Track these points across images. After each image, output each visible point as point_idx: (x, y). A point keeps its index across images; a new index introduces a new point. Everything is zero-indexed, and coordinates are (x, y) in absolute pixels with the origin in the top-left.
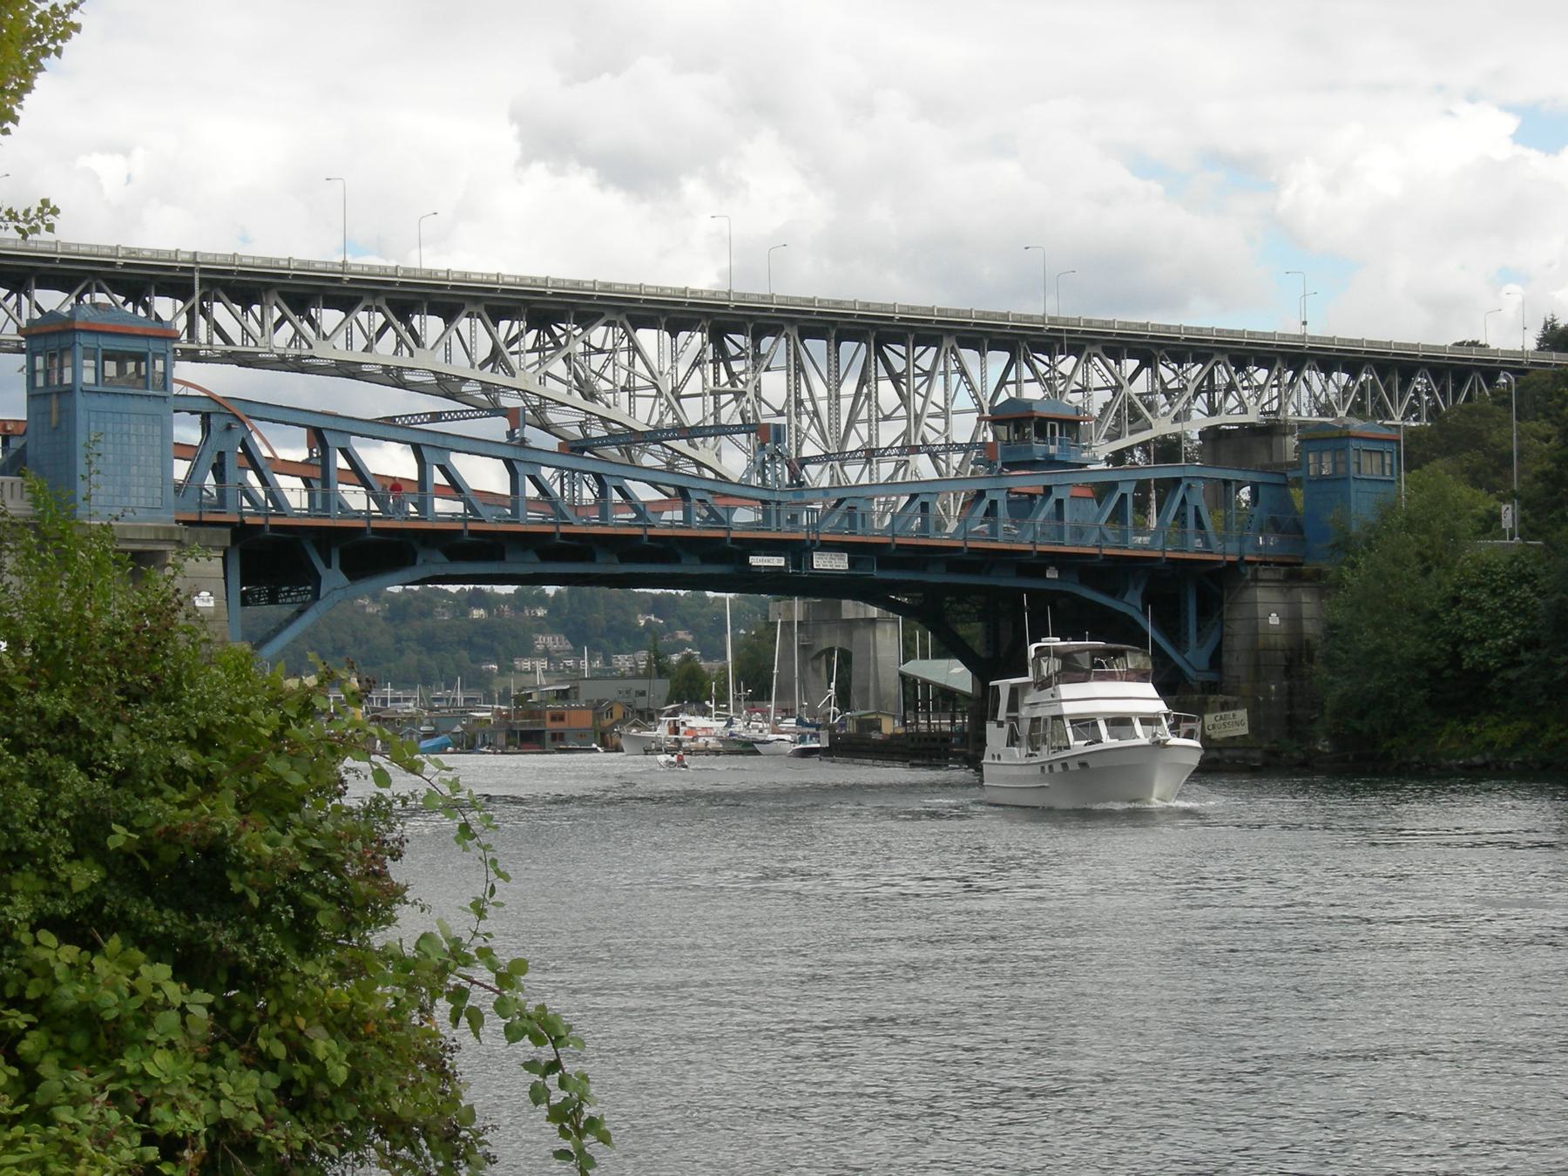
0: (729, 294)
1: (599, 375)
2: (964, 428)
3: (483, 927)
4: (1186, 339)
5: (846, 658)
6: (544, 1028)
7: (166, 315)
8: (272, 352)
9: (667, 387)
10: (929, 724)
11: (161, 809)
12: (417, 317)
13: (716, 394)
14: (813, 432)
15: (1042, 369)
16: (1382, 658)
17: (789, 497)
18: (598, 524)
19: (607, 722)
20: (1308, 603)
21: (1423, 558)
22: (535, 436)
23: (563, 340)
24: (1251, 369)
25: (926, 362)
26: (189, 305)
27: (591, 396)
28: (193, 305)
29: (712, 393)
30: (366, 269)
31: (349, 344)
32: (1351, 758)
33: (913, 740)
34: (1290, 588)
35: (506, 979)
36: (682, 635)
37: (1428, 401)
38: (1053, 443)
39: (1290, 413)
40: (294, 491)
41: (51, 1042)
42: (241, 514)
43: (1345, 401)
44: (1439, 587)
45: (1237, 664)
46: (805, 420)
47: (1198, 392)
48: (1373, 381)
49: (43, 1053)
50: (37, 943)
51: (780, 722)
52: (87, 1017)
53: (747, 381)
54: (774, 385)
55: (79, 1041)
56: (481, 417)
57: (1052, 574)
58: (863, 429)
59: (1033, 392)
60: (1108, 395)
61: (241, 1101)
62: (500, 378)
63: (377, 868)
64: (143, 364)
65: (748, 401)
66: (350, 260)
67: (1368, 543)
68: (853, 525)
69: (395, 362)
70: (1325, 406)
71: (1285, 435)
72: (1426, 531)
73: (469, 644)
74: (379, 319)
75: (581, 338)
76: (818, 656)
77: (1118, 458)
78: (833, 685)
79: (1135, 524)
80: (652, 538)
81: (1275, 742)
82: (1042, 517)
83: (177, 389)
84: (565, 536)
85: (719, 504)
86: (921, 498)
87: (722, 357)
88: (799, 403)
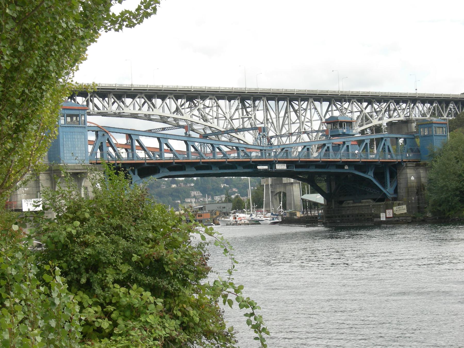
0: (245, 89)
1: (208, 114)
2: (316, 126)
3: (231, 277)
4: (381, 96)
5: (285, 194)
6: (251, 304)
7: (80, 103)
8: (112, 112)
9: (228, 117)
10: (311, 213)
11: (145, 249)
12: (154, 99)
13: (243, 118)
14: (272, 128)
15: (339, 106)
16: (446, 188)
17: (268, 148)
18: (212, 159)
19: (215, 216)
20: (422, 172)
21: (456, 158)
22: (193, 134)
23: (197, 104)
24: (401, 104)
25: (304, 106)
26: (87, 99)
27: (206, 120)
28: (88, 99)
29: (242, 118)
30: (138, 86)
31: (134, 108)
32: (437, 218)
33: (307, 218)
34: (417, 169)
35: (237, 291)
36: (234, 190)
37: (454, 111)
38: (345, 129)
39: (413, 116)
40: (124, 155)
41: (120, 314)
42: (108, 160)
43: (429, 112)
44: (461, 166)
45: (402, 192)
46: (269, 125)
47: (385, 111)
48: (437, 106)
49: (118, 317)
50: (114, 287)
51: (266, 214)
52: (130, 307)
53: (252, 114)
54: (260, 115)
55: (128, 313)
56: (177, 129)
57: (346, 167)
58: (287, 127)
59: (337, 114)
60: (359, 113)
61: (171, 328)
62: (179, 116)
63: (204, 263)
64: (78, 118)
65: (252, 120)
66: (133, 84)
67: (440, 154)
68: (287, 155)
69: (148, 113)
70: (423, 114)
71: (412, 123)
72: (457, 150)
73: (172, 195)
74: (143, 100)
75: (202, 103)
76: (277, 194)
77: (362, 132)
78: (281, 203)
79: (370, 152)
80: (228, 162)
81: (415, 214)
82: (343, 151)
83: (88, 124)
84: (203, 162)
85: (247, 151)
86: (306, 147)
87: (244, 107)
88: (267, 120)
